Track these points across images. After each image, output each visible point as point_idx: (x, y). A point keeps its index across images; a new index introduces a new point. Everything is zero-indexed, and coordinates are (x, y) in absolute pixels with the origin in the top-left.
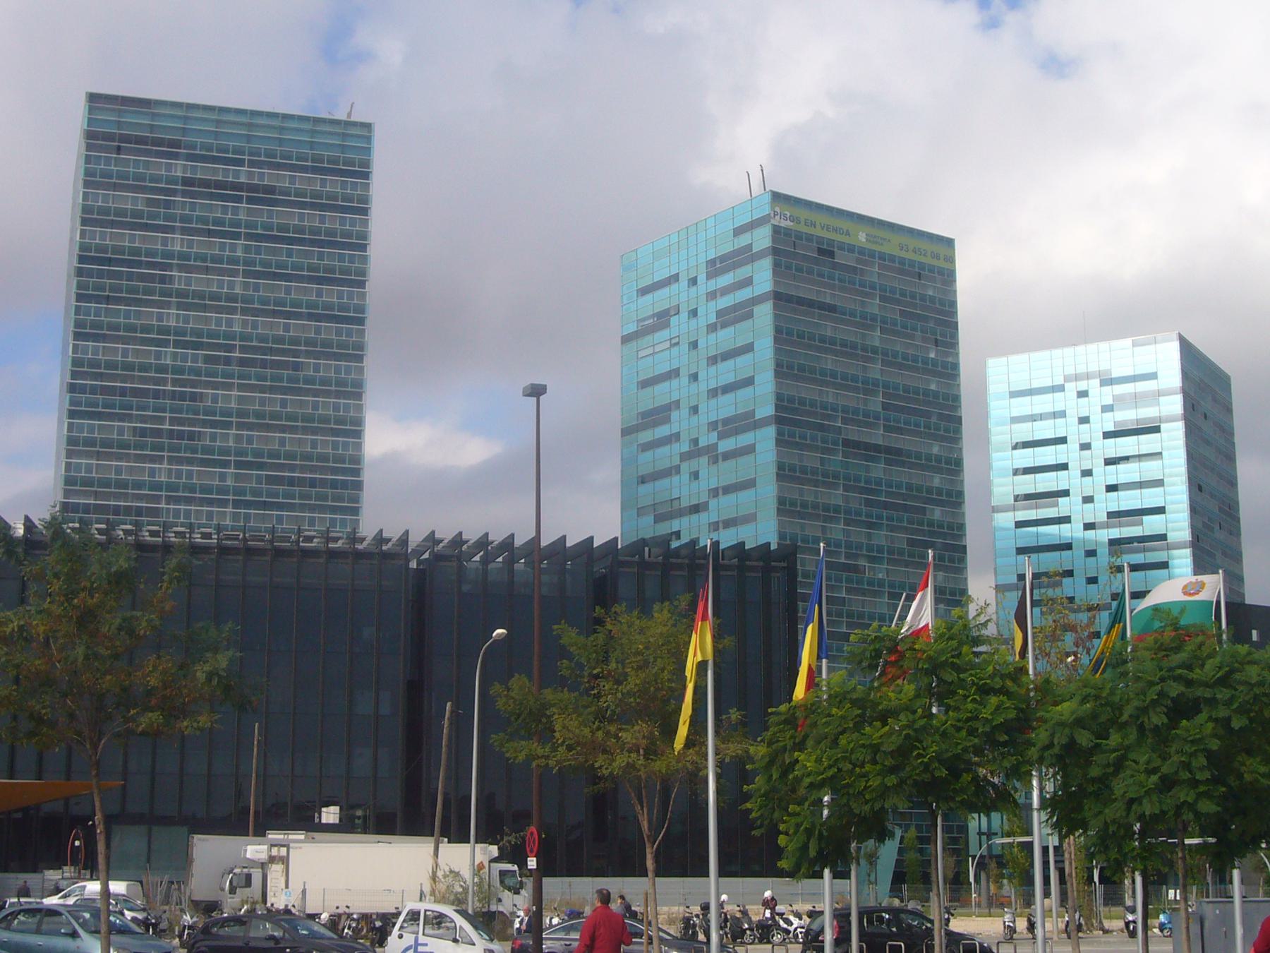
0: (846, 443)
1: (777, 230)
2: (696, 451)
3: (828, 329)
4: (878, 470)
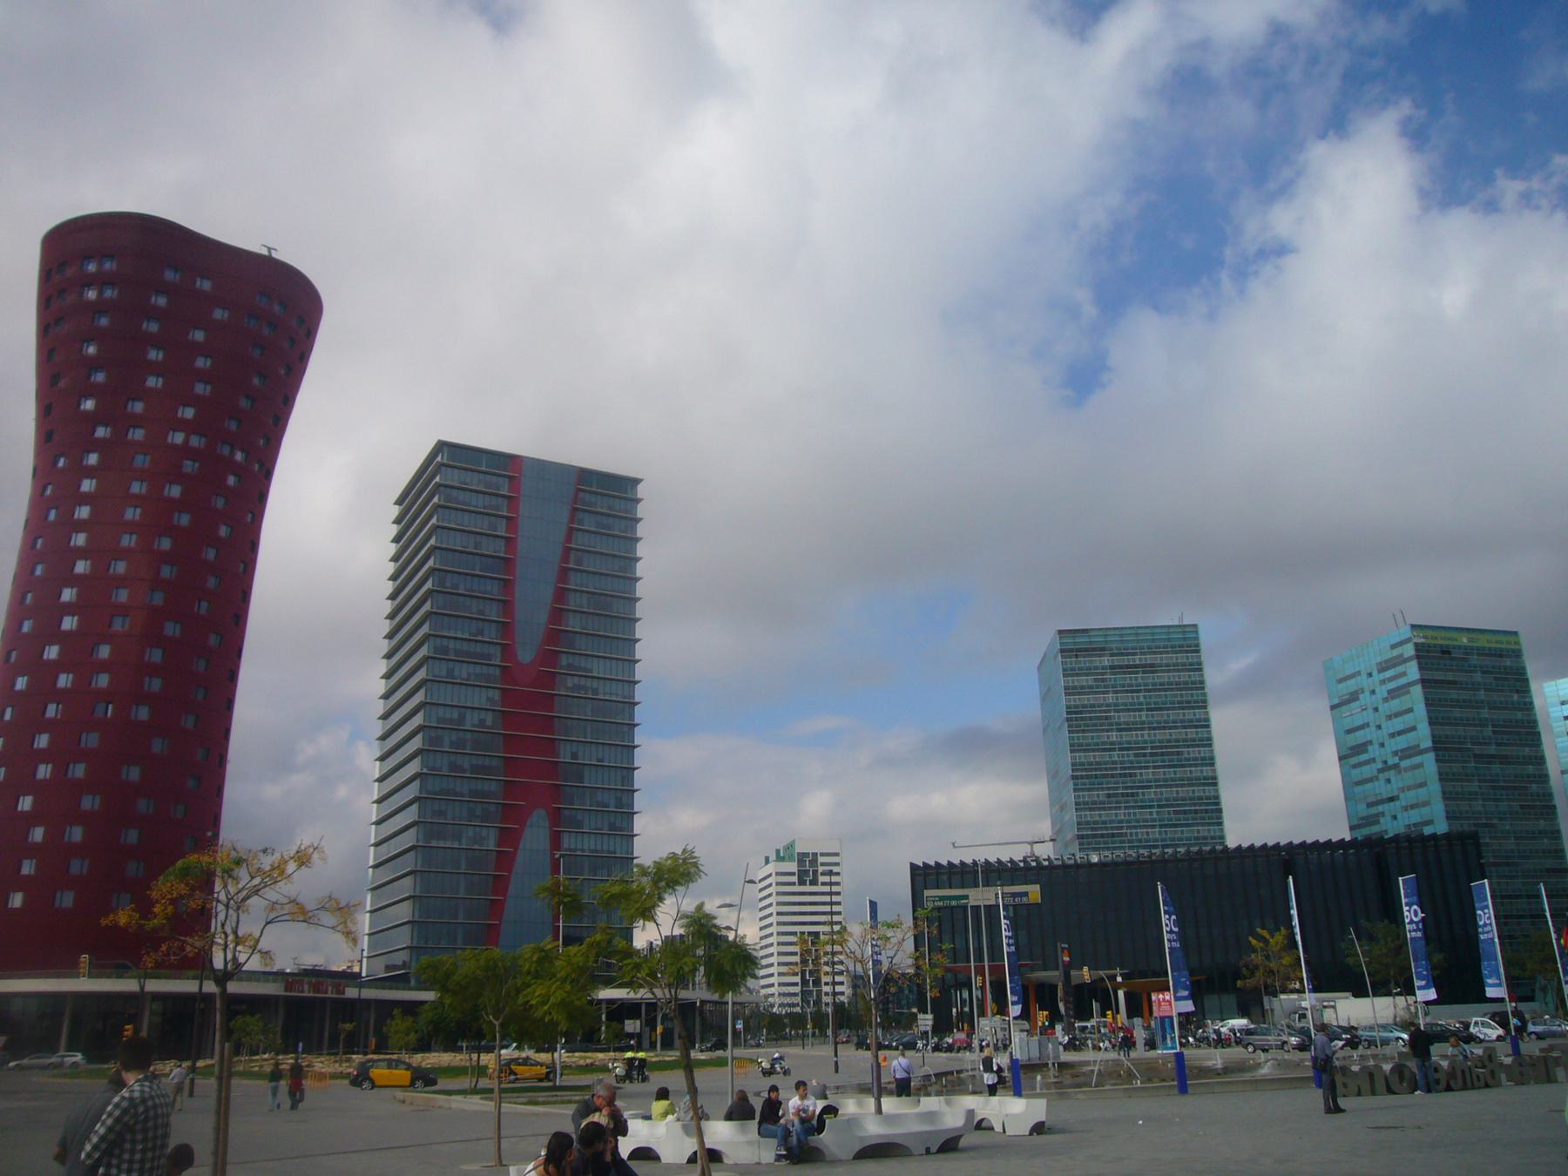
0: (1475, 756)
1: (1416, 645)
2: (1386, 767)
3: (1454, 694)
4: (1496, 768)
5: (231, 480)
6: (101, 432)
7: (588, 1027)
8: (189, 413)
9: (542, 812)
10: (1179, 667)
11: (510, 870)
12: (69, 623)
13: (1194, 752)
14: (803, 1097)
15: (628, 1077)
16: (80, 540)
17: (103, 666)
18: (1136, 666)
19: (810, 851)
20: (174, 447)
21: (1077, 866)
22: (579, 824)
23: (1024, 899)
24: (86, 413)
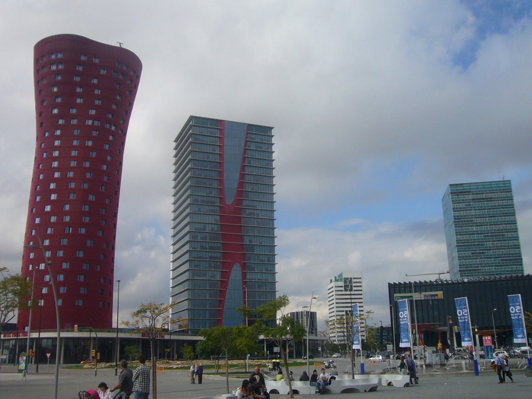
5: (111, 138)
6: (61, 122)
7: (257, 350)
8: (93, 112)
9: (238, 264)
10: (502, 199)
11: (226, 288)
12: (53, 197)
13: (510, 235)
14: (324, 373)
15: (274, 369)
16: (55, 164)
17: (67, 213)
18: (484, 199)
19: (349, 277)
20: (88, 126)
21: (458, 283)
22: (253, 269)
23: (436, 297)
24: (55, 114)
